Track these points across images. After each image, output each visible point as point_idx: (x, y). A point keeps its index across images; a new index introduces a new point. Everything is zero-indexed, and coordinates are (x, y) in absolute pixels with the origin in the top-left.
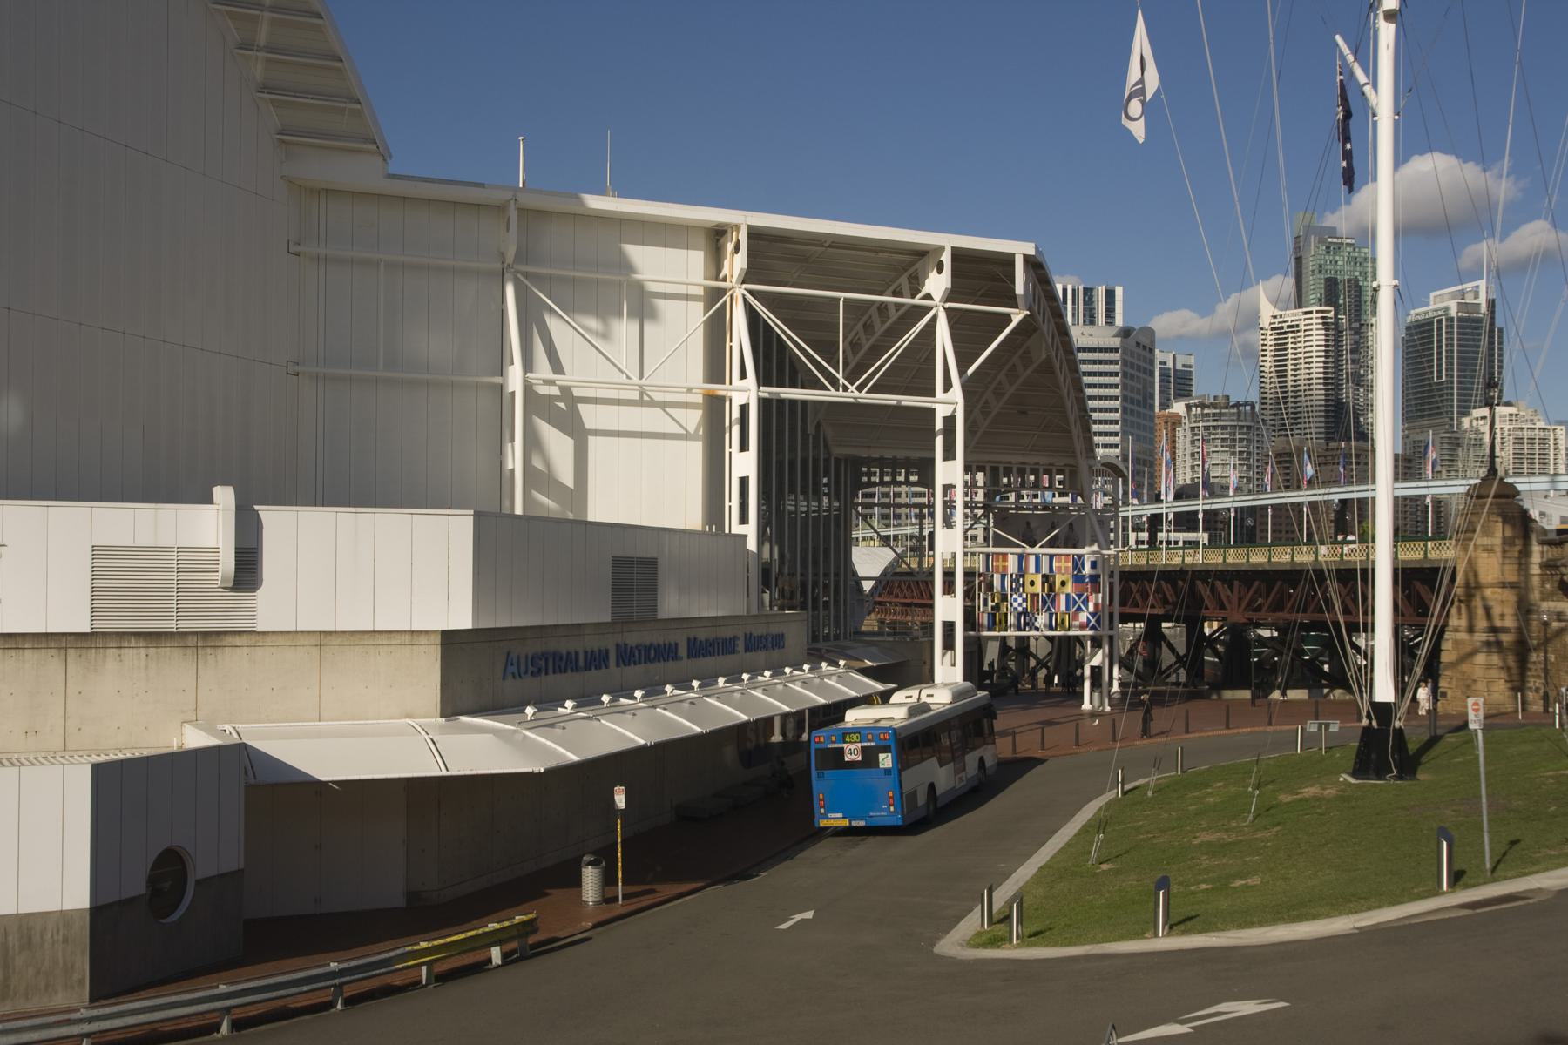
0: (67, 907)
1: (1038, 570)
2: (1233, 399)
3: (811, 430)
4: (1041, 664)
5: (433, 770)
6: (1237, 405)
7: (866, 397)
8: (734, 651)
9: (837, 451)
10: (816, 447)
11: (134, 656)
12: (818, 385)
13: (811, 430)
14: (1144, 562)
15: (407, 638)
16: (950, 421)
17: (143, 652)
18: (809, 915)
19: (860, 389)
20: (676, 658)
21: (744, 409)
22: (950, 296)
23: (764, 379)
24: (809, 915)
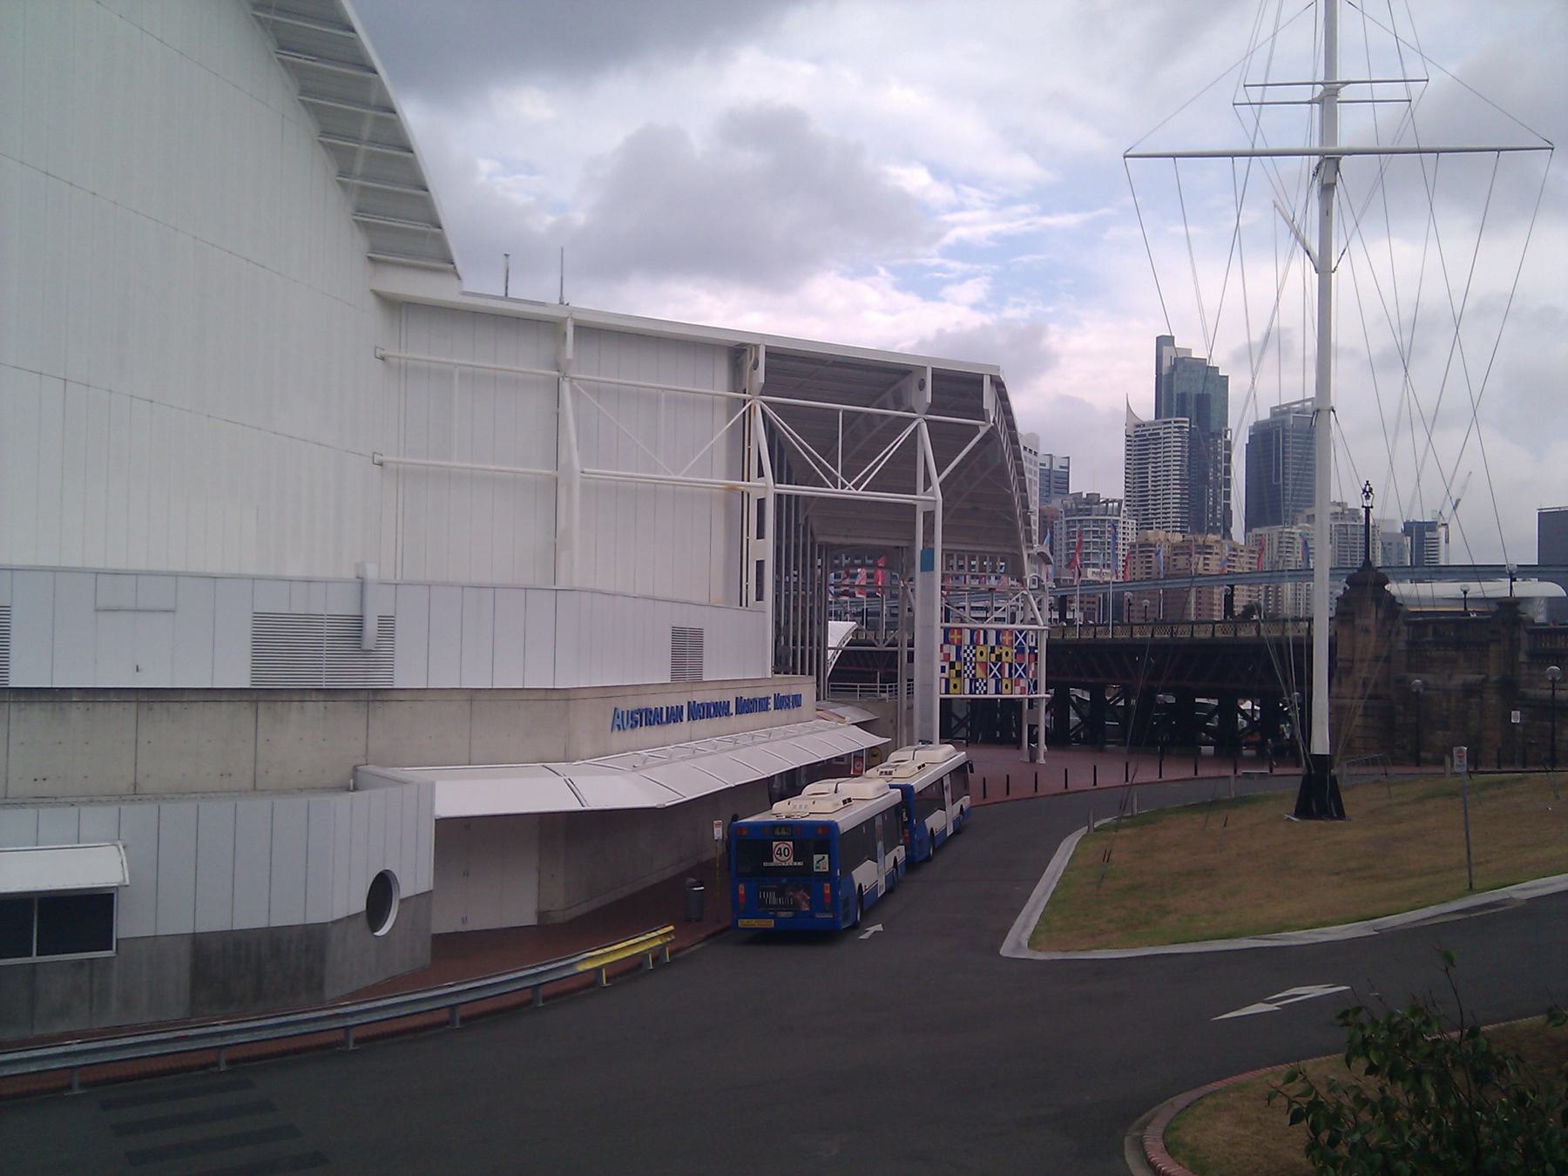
0: (201, 929)
1: (986, 641)
2: (1103, 497)
3: (801, 521)
4: (962, 723)
5: (573, 805)
6: (1107, 502)
7: (860, 494)
8: (767, 709)
9: (820, 539)
10: (805, 535)
11: (314, 709)
12: (823, 485)
13: (801, 521)
14: (1187, 635)
15: (541, 695)
16: (929, 516)
17: (321, 705)
18: (879, 927)
19: (857, 486)
20: (728, 714)
21: (761, 503)
22: (934, 408)
23: (778, 479)
24: (879, 927)
